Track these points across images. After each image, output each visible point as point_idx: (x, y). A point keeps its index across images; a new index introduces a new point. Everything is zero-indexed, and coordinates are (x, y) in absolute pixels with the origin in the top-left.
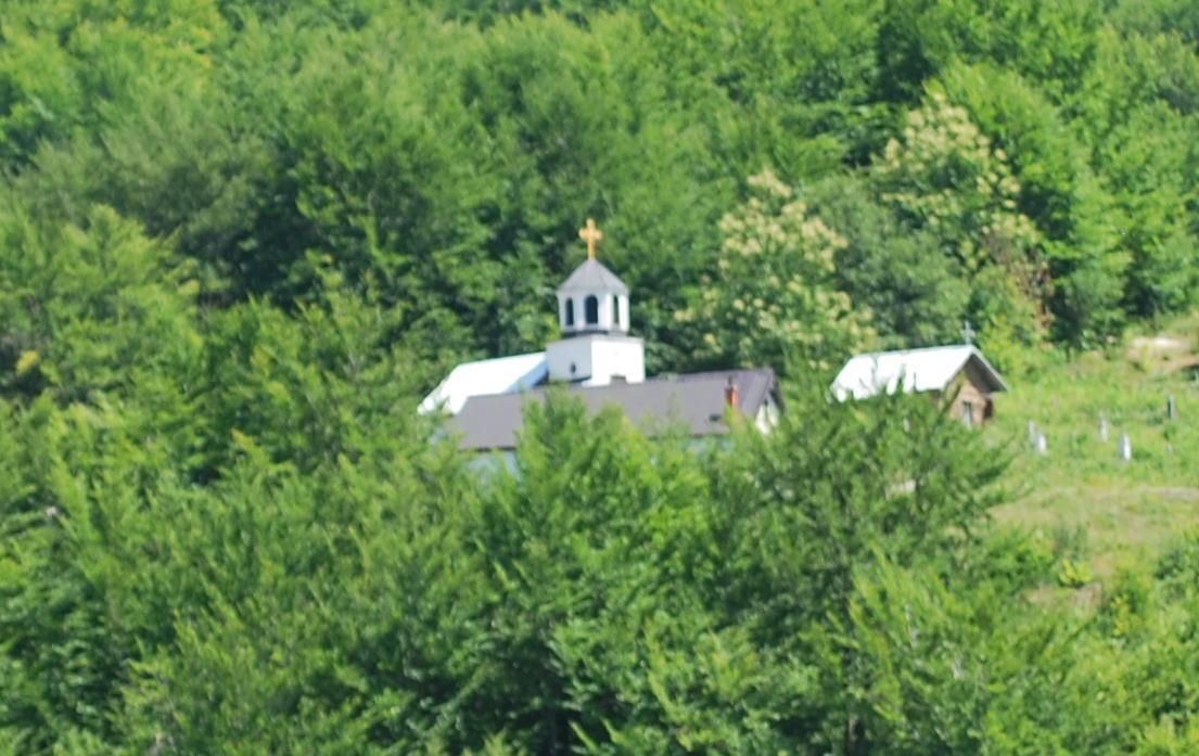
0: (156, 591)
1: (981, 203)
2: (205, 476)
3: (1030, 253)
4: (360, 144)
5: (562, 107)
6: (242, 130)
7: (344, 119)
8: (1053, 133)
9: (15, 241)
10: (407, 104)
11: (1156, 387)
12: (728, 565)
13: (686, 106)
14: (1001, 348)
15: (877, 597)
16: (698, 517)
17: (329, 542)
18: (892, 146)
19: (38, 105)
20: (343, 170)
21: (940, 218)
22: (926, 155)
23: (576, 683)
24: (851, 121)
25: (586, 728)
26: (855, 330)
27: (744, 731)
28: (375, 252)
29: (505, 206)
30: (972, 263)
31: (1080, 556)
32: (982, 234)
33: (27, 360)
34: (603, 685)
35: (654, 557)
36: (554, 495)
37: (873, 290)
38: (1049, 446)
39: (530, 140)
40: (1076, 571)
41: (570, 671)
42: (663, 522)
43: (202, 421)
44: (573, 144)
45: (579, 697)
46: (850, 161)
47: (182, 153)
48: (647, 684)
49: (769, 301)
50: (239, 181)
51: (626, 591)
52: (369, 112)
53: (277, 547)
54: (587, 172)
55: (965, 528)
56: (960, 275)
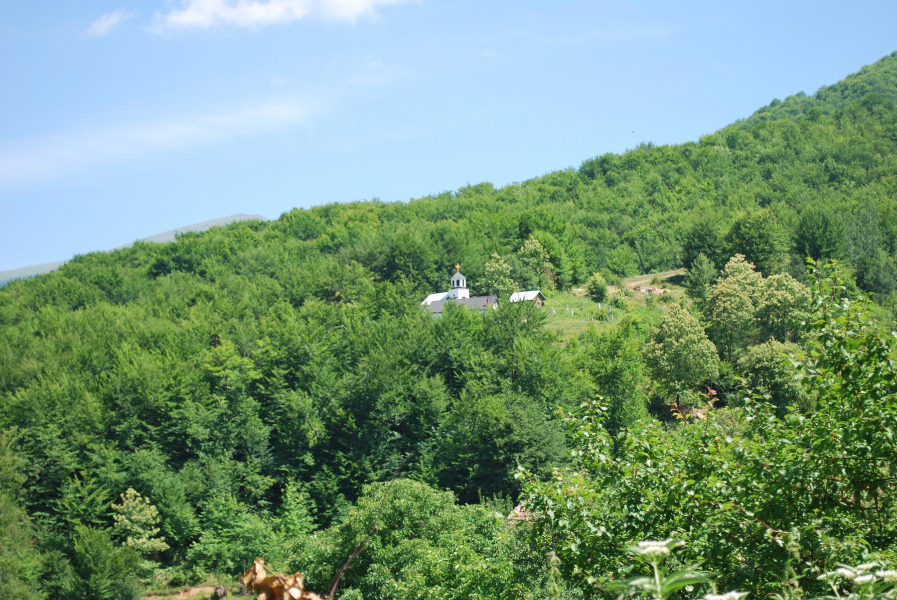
3: (552, 271)
7: (405, 242)
8: (557, 245)
16: (481, 327)
39: (445, 246)
42: (473, 328)
44: (454, 247)
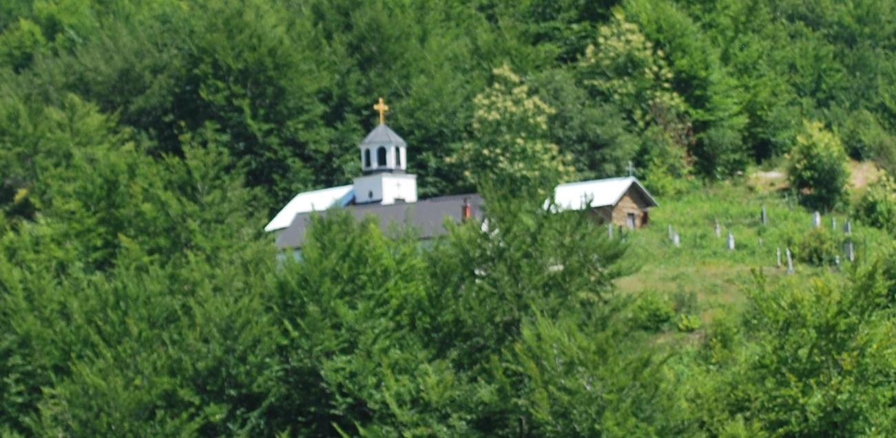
0: (64, 342)
1: (648, 85)
2: (102, 265)
3: (681, 117)
4: (241, 52)
5: (374, 26)
6: (165, 45)
7: (230, 36)
8: (695, 38)
9: (14, 118)
10: (275, 26)
11: (759, 202)
12: (439, 319)
13: (458, 25)
14: (659, 179)
15: (535, 338)
16: (419, 289)
17: (177, 307)
18: (590, 50)
19: (72, 33)
20: (229, 69)
21: (621, 95)
22: (612, 54)
23: (338, 397)
24: (567, 33)
25: (344, 428)
26: (561, 168)
27: (449, 427)
28: (250, 121)
29: (336, 91)
30: (641, 124)
31: (693, 312)
32: (648, 105)
33: (21, 194)
34: (355, 398)
35: (391, 313)
36: (323, 275)
37: (575, 142)
38: (681, 241)
39: (353, 48)
40: (689, 321)
41: (334, 389)
42: (397, 290)
43: (102, 230)
44: (382, 51)
45: (340, 405)
46: (562, 59)
47: (126, 60)
48: (383, 397)
49: (505, 149)
50: (161, 78)
51: (371, 336)
52: (247, 32)
53: (144, 312)
54: (390, 69)
55: (597, 293)
56: (631, 132)
